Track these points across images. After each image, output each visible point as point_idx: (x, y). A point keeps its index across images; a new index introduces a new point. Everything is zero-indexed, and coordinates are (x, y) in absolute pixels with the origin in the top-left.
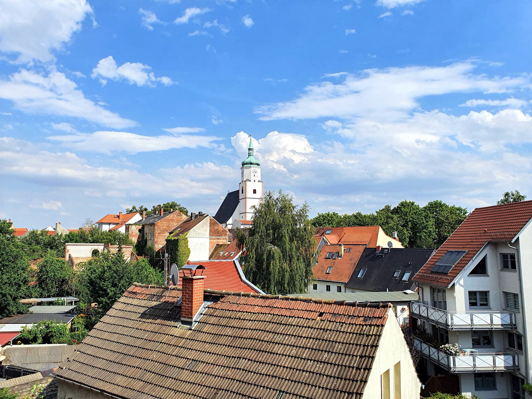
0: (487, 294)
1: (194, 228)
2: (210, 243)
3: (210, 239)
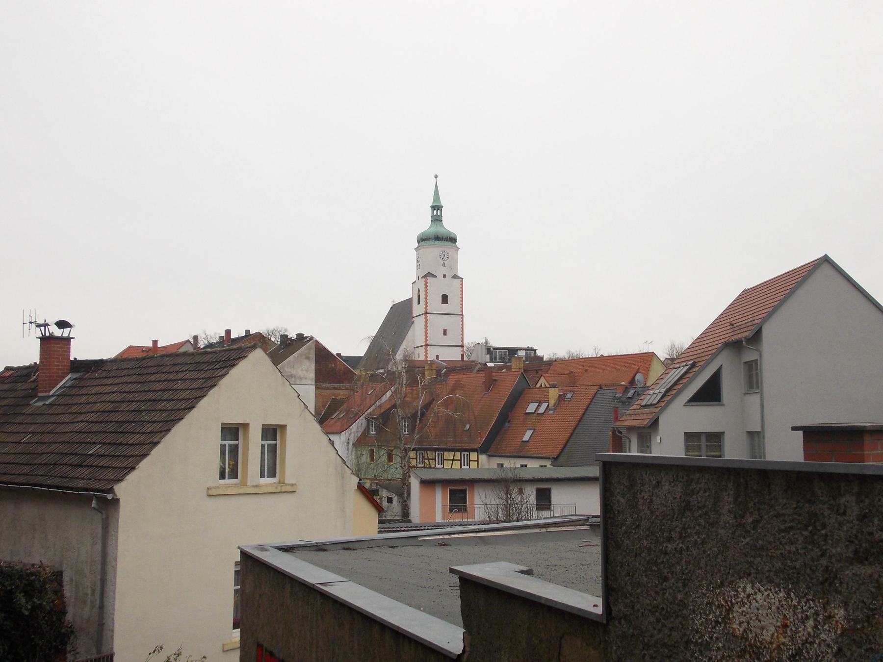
0: (276, 431)
1: (661, 454)
3: (317, 388)
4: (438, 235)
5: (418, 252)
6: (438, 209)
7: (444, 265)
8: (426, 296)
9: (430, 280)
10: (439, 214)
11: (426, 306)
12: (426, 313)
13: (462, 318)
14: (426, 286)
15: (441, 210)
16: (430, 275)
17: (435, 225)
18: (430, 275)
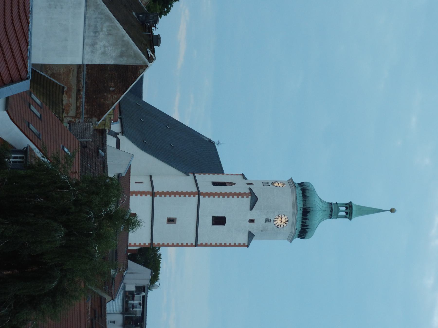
2: (69, 68)
3: (79, 66)
5: (287, 183)
6: (347, 213)
8: (224, 195)
9: (247, 201)
10: (341, 214)
11: (210, 194)
12: (199, 194)
13: (192, 245)
14: (238, 195)
15: (346, 217)
16: (254, 200)
17: (324, 209)
18: (254, 200)
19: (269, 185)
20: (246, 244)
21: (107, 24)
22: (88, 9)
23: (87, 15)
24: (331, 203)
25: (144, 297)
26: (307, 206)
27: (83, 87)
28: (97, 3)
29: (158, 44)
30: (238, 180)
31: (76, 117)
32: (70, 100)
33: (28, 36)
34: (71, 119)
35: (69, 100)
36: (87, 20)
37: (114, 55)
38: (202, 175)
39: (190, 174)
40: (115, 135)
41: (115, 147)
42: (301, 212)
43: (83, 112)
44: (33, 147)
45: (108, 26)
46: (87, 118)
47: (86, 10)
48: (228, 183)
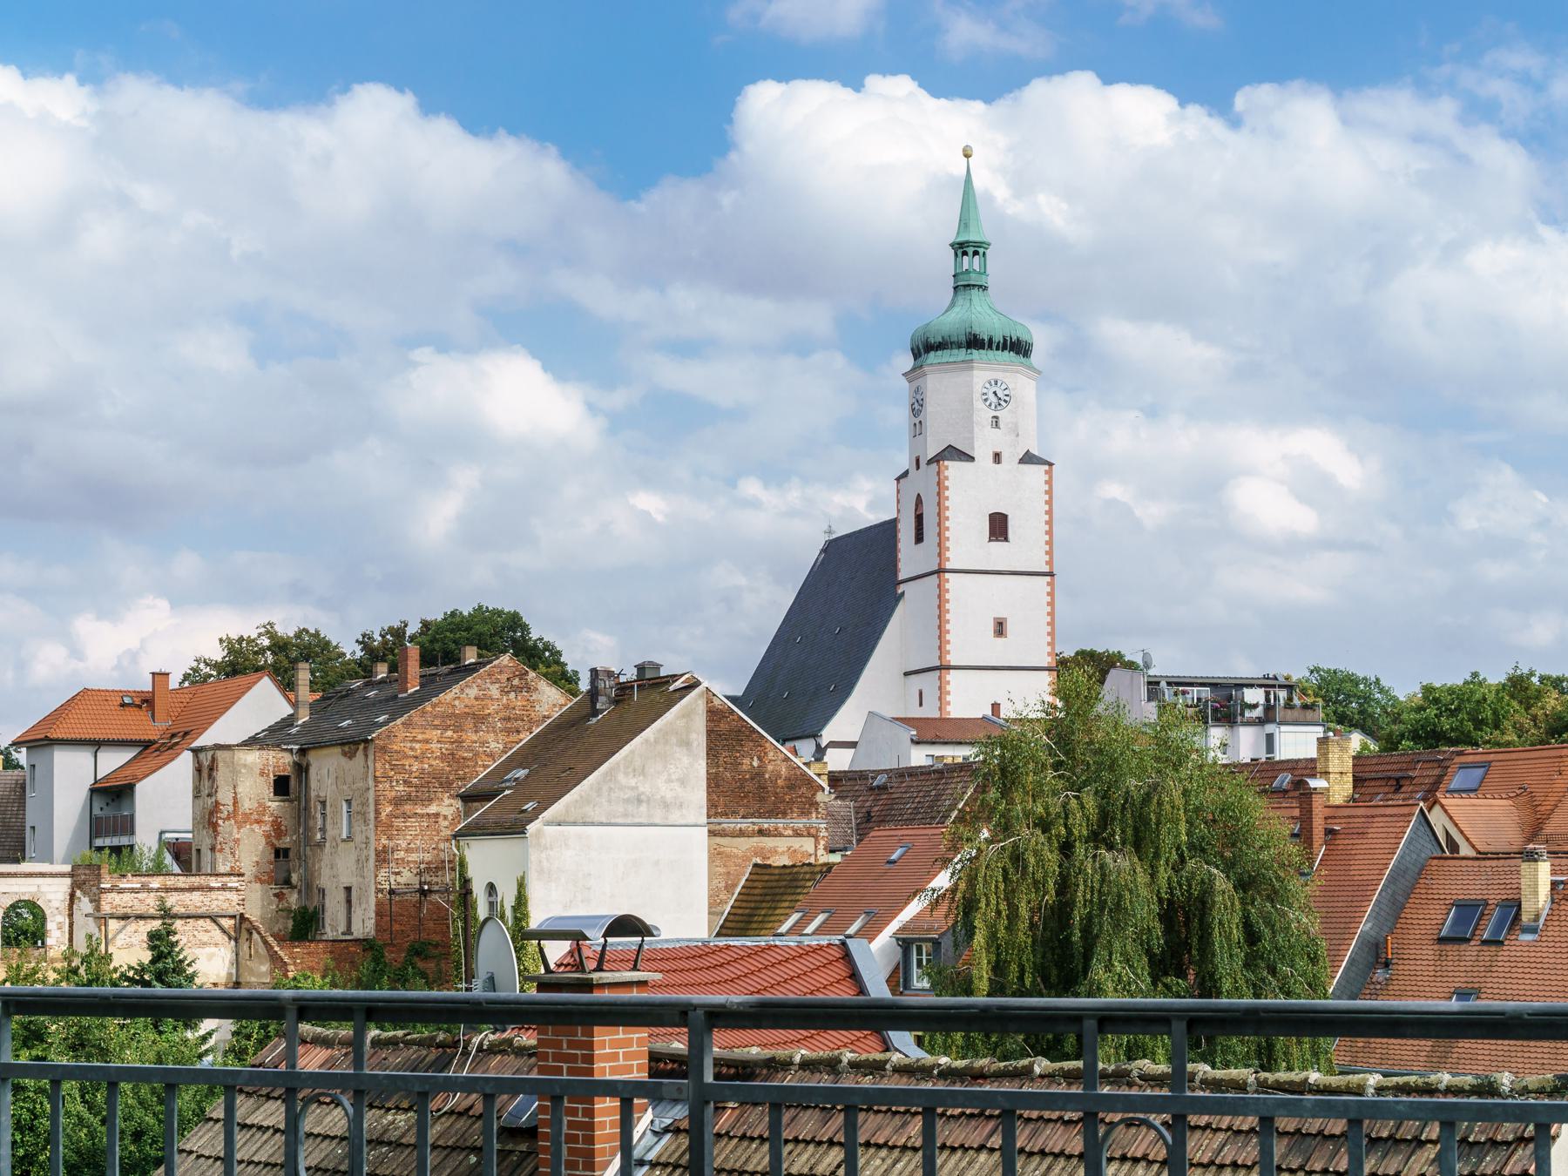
2: (715, 855)
3: (712, 833)
4: (21, 79)
5: (915, 384)
6: (975, 253)
7: (996, 422)
9: (953, 468)
10: (976, 267)
19: (920, 422)
20: (1047, 467)
21: (621, 777)
22: (590, 820)
23: (604, 820)
24: (955, 288)
25: (1169, 684)
26: (963, 339)
27: (754, 823)
28: (577, 801)
29: (657, 667)
30: (913, 486)
31: (816, 837)
32: (780, 850)
33: (747, 947)
34: (821, 847)
35: (783, 853)
36: (613, 821)
37: (686, 760)
38: (901, 565)
39: (900, 591)
40: (820, 753)
41: (853, 750)
42: (974, 351)
43: (805, 820)
44: (894, 926)
45: (626, 774)
46: (818, 813)
47: (593, 824)
48: (916, 510)
